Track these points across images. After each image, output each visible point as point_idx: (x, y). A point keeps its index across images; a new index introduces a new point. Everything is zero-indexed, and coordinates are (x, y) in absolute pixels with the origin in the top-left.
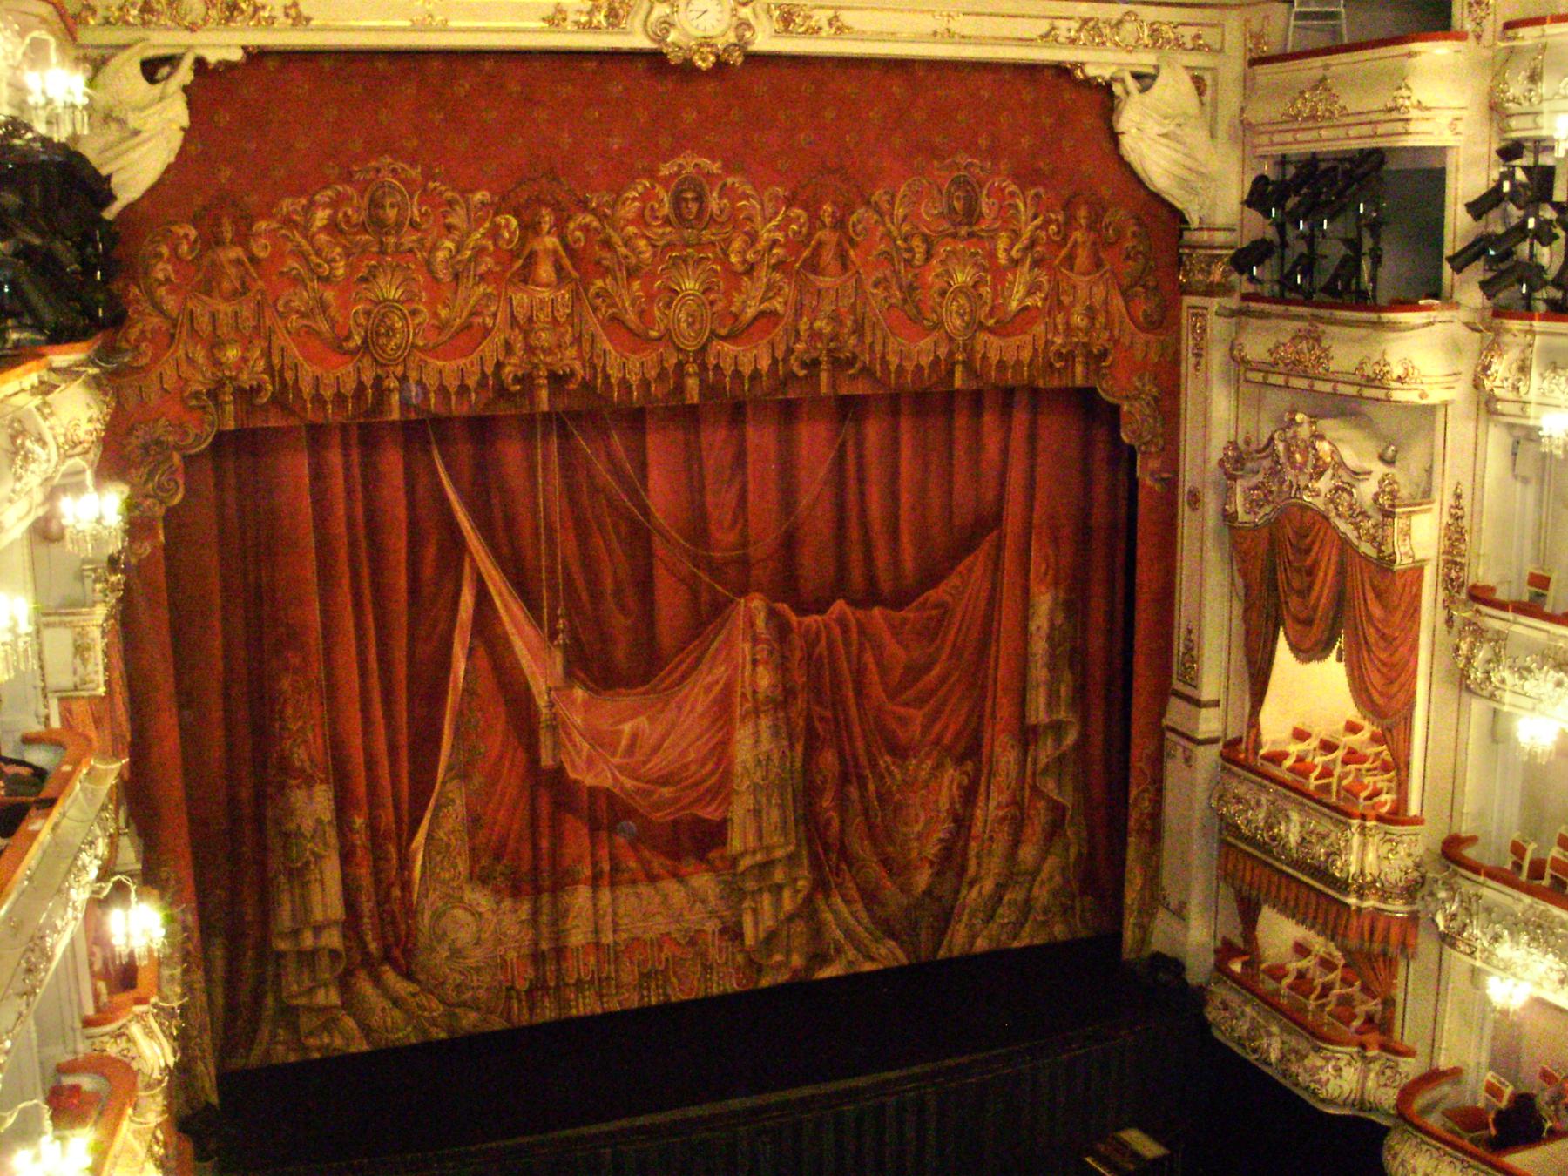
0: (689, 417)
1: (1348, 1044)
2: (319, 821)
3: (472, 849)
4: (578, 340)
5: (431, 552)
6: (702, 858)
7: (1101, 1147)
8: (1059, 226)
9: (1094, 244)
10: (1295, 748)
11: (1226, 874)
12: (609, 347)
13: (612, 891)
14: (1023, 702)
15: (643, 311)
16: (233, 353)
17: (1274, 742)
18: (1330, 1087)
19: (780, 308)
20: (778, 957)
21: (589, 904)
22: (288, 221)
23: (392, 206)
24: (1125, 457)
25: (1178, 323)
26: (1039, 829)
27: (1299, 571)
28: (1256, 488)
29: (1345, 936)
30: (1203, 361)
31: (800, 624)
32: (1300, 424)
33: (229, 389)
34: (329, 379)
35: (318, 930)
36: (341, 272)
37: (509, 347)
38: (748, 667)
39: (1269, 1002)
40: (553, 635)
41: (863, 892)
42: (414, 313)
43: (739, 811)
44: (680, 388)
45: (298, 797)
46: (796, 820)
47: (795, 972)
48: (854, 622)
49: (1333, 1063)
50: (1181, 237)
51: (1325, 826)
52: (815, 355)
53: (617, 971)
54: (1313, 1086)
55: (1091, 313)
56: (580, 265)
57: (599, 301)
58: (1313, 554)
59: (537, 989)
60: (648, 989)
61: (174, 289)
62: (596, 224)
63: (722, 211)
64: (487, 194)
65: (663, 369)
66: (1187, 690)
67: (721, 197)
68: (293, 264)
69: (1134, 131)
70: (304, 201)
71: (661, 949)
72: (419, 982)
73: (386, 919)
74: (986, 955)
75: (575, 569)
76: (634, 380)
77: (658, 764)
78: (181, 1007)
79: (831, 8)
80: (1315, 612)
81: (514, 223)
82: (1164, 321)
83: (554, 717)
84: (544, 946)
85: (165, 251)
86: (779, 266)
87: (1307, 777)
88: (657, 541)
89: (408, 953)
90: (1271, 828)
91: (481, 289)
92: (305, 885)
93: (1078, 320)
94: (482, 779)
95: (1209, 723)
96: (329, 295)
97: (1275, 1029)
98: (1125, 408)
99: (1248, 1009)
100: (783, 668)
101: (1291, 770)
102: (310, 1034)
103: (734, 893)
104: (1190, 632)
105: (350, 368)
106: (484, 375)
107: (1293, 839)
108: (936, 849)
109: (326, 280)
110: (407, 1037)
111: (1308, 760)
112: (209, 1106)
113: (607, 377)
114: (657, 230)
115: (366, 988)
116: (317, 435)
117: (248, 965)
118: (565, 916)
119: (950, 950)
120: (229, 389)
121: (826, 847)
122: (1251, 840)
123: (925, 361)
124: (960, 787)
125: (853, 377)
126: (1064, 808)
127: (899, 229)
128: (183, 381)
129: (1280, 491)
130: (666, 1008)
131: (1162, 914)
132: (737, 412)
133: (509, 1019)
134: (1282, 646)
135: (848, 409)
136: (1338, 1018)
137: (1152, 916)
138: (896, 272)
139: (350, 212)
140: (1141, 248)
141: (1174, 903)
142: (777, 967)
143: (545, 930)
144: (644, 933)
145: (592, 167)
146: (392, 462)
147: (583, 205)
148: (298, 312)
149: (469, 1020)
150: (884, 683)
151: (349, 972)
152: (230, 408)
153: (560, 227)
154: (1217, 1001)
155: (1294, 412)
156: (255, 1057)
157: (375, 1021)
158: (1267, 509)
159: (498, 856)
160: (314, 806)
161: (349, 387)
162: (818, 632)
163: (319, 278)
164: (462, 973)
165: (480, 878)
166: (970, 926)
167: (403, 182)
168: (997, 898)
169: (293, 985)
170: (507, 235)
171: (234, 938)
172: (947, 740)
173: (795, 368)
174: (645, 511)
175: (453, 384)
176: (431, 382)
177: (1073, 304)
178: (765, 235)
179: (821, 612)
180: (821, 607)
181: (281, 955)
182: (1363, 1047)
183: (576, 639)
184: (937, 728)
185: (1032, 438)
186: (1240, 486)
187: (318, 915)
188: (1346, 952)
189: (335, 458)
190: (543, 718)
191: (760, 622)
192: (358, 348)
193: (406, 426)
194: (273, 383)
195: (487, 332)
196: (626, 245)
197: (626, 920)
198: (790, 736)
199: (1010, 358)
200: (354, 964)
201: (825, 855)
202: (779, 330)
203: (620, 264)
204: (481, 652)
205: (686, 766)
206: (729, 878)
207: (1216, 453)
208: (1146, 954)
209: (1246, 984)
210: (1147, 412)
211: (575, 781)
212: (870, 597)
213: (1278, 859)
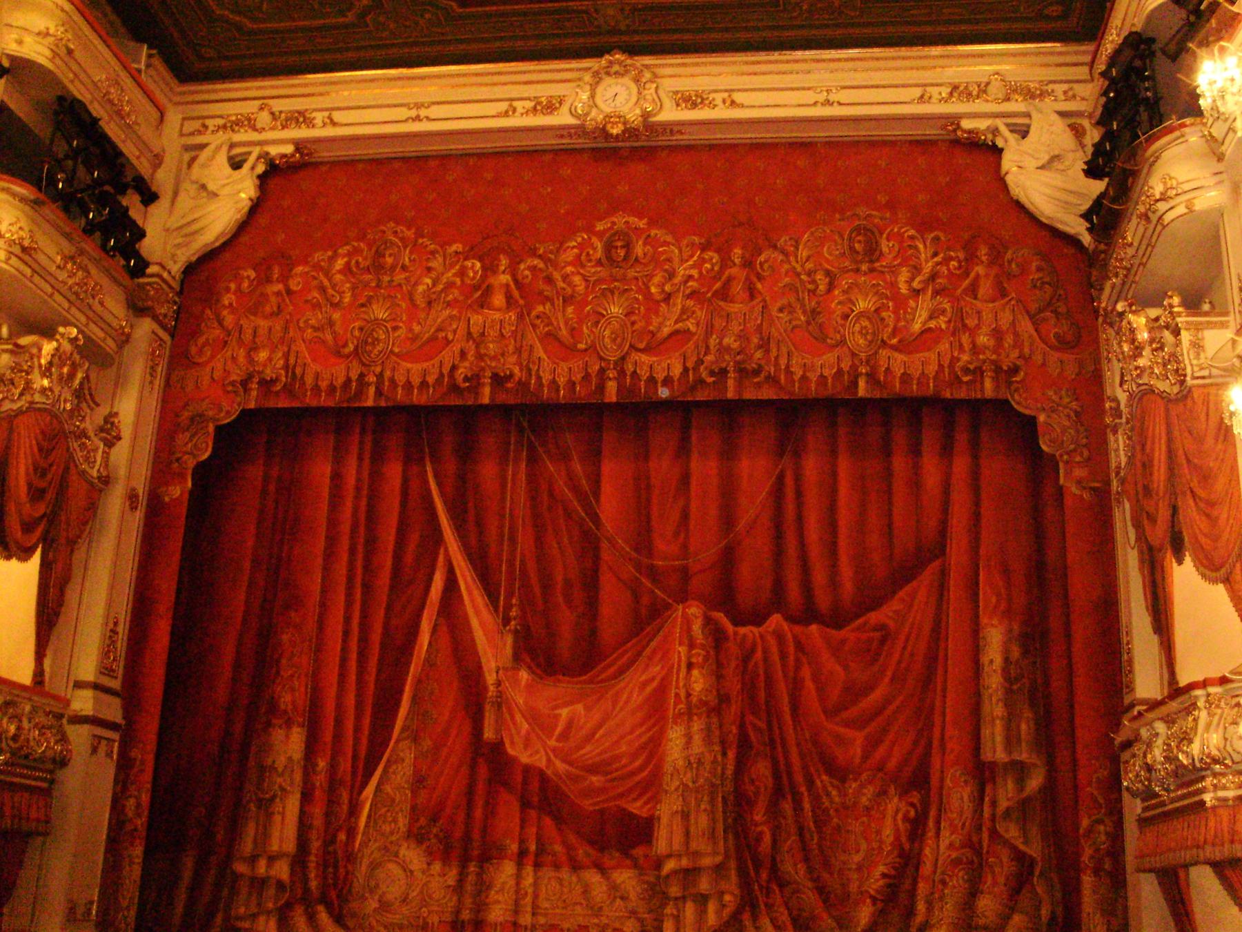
2: (290, 759)
3: (413, 808)
4: (518, 351)
5: (414, 538)
6: (626, 853)
8: (960, 262)
12: (544, 356)
13: (535, 872)
14: (977, 737)
15: (573, 329)
16: (263, 355)
19: (693, 328)
21: (512, 882)
22: (317, 267)
23: (390, 255)
26: (1002, 880)
31: (736, 634)
33: (256, 380)
34: (327, 376)
35: (272, 859)
36: (347, 300)
37: (463, 354)
40: (506, 621)
42: (395, 329)
43: (667, 809)
44: (601, 388)
45: (278, 735)
48: (789, 635)
52: (724, 365)
55: (998, 334)
56: (524, 296)
62: (542, 265)
67: (645, 244)
69: (1015, 169)
70: (330, 253)
73: (328, 860)
75: (531, 566)
76: (562, 381)
77: (590, 752)
79: (726, 91)
81: (478, 265)
84: (466, 915)
85: (233, 286)
86: (693, 295)
88: (605, 544)
89: (344, 897)
92: (270, 815)
94: (429, 743)
96: (336, 316)
98: (1042, 418)
100: (718, 675)
105: (343, 366)
106: (441, 375)
109: (335, 306)
113: (539, 378)
114: (591, 269)
118: (489, 887)
120: (256, 380)
121: (758, 865)
124: (906, 818)
126: (1032, 861)
127: (802, 266)
140: (1047, 280)
143: (468, 902)
145: (542, 226)
147: (534, 253)
148: (313, 327)
150: (823, 699)
151: (288, 906)
152: (254, 393)
159: (434, 819)
160: (289, 745)
162: (754, 646)
163: (332, 304)
165: (416, 836)
172: (892, 764)
173: (704, 375)
174: (596, 520)
176: (401, 379)
177: (978, 327)
178: (681, 272)
180: (758, 619)
181: (237, 877)
183: (527, 628)
184: (881, 750)
185: (975, 475)
187: (275, 847)
191: (697, 628)
194: (287, 377)
195: (448, 342)
196: (564, 281)
198: (724, 744)
202: (691, 344)
205: (618, 758)
206: (652, 879)
210: (1067, 423)
212: (808, 614)
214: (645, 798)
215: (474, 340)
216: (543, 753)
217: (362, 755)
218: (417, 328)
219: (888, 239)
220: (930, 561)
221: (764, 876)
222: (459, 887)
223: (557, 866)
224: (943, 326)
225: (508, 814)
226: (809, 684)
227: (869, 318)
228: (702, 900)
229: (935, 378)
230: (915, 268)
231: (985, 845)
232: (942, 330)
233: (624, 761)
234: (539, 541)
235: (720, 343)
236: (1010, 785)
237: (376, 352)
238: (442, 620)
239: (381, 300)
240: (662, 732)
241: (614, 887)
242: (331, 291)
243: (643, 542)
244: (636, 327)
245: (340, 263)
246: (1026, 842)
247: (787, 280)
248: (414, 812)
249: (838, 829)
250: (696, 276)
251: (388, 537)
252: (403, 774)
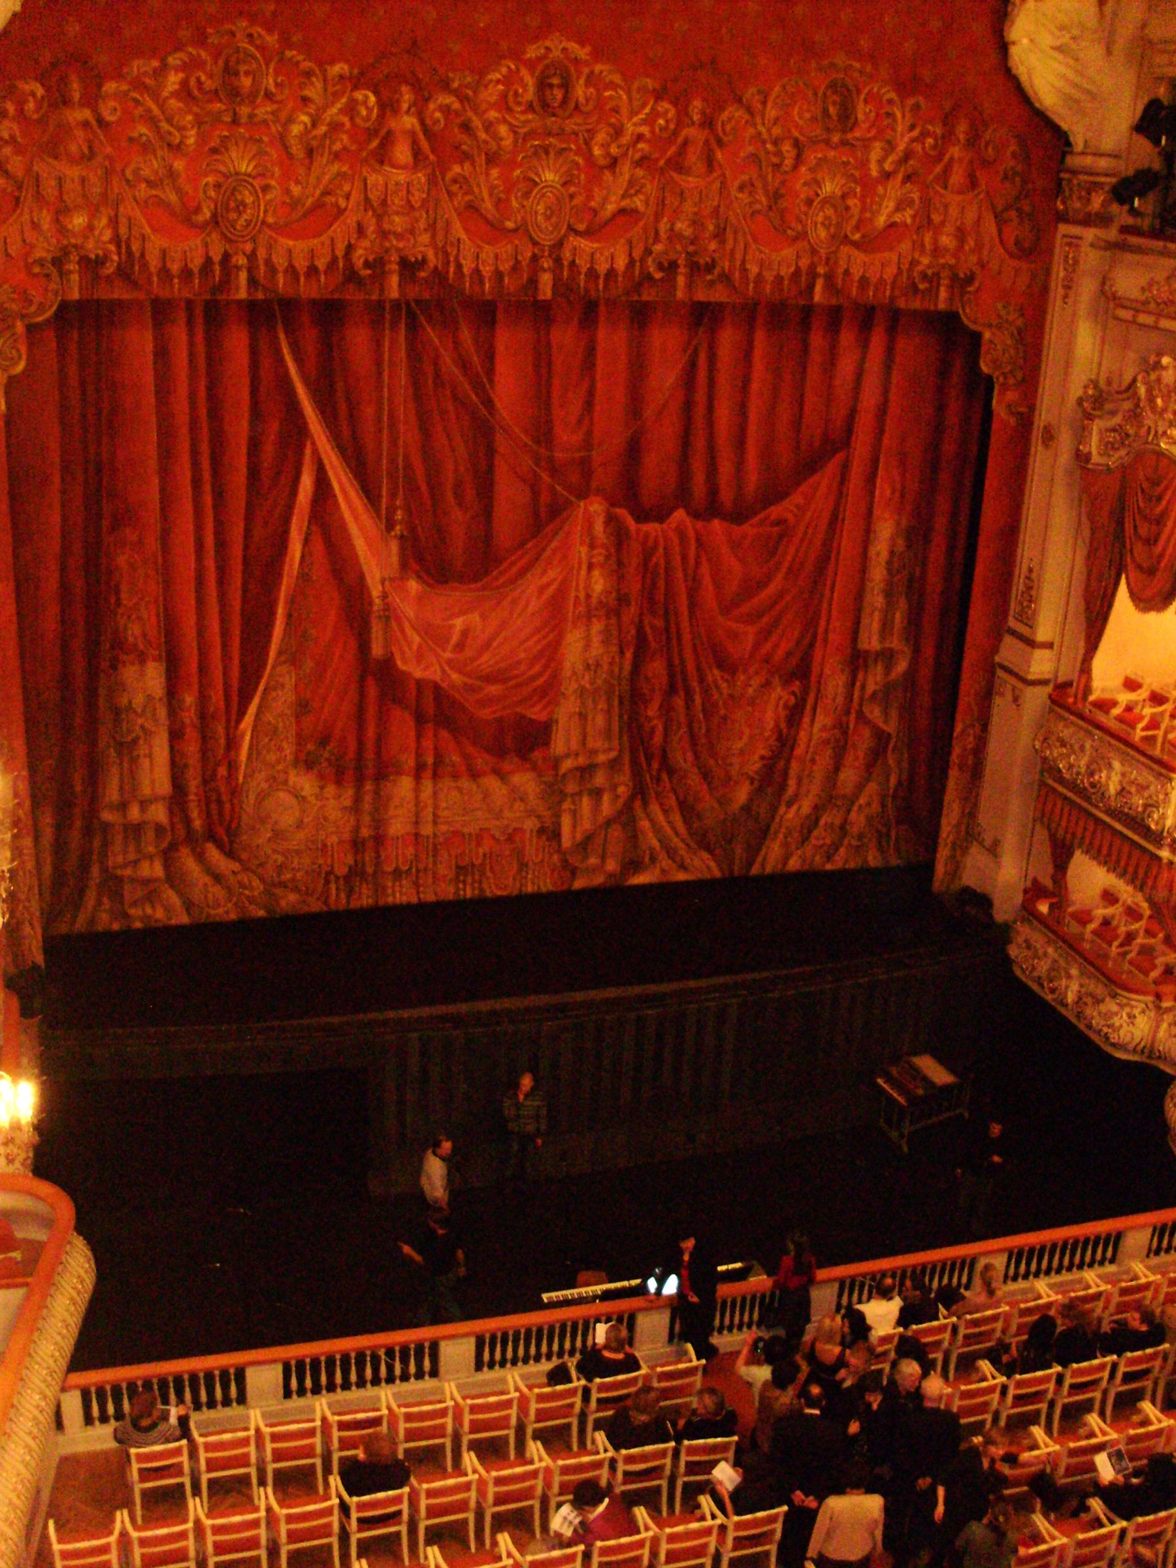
0: (541, 314)
1: (1144, 993)
3: (299, 735)
4: (432, 227)
7: (894, 1071)
9: (971, 162)
10: (1124, 698)
11: (1043, 816)
12: (463, 236)
16: (79, 221)
17: (1103, 690)
18: (1122, 1033)
20: (593, 861)
22: (138, 84)
23: (247, 73)
24: (980, 389)
25: (1050, 252)
26: (861, 754)
27: (1146, 519)
28: (1114, 430)
29: (1154, 887)
30: (1071, 293)
31: (638, 531)
32: (1165, 368)
33: (74, 257)
35: (144, 804)
37: (361, 230)
38: (584, 572)
39: (1072, 946)
40: (390, 526)
41: (682, 804)
42: (266, 189)
43: (565, 712)
44: (533, 282)
45: (129, 673)
46: (621, 728)
47: (611, 875)
49: (1127, 1009)
50: (1062, 161)
51: (1145, 777)
53: (435, 863)
54: (1105, 1030)
55: (961, 234)
56: (438, 150)
57: (455, 188)
58: (1164, 503)
59: (355, 873)
60: (464, 882)
61: (19, 150)
62: (457, 106)
63: (587, 100)
64: (346, 67)
65: (518, 262)
66: (1021, 628)
69: (1025, 41)
70: (155, 63)
71: (478, 844)
72: (239, 860)
73: (210, 799)
74: (798, 875)
76: (487, 270)
77: (487, 661)
78: (10, 871)
80: (1159, 563)
82: (1035, 251)
83: (387, 607)
84: (365, 832)
85: (11, 108)
87: (1134, 728)
89: (232, 832)
90: (1092, 774)
91: (335, 168)
92: (134, 761)
93: (946, 240)
95: (1041, 664)
96: (179, 165)
97: (1074, 972)
98: (987, 335)
99: (1050, 950)
100: (618, 573)
101: (1119, 719)
102: (134, 904)
103: (554, 793)
104: (1031, 570)
105: (198, 242)
106: (334, 259)
107: (1113, 789)
108: (758, 765)
109: (176, 149)
110: (227, 912)
111: (1137, 710)
112: (35, 967)
113: (459, 266)
115: (190, 864)
116: (161, 310)
117: (75, 838)
119: (763, 866)
120: (74, 257)
121: (649, 757)
122: (1072, 786)
123: (786, 271)
124: (786, 706)
125: (711, 283)
127: (769, 130)
128: (28, 247)
129: (1136, 434)
130: (481, 903)
131: (974, 849)
132: (589, 312)
133: (326, 903)
134: (1123, 592)
135: (703, 316)
136: (1138, 967)
137: (965, 851)
138: (763, 177)
139: (203, 78)
141: (987, 843)
142: (594, 870)
143: (366, 819)
144: (466, 829)
146: (237, 341)
147: (446, 86)
148: (147, 181)
149: (289, 901)
151: (173, 847)
152: (75, 278)
154: (1020, 940)
155: (1160, 354)
156: (81, 924)
157: (196, 895)
158: (1123, 452)
160: (145, 682)
161: (196, 263)
164: (283, 854)
165: (308, 764)
166: (786, 845)
167: (257, 48)
168: (812, 822)
169: (118, 856)
170: (364, 112)
171: (64, 808)
174: (489, 403)
175: (301, 264)
176: (280, 261)
177: (943, 223)
178: (630, 128)
179: (661, 519)
181: (106, 827)
182: (1159, 997)
183: (412, 529)
184: (768, 646)
186: (1096, 427)
188: (1153, 904)
189: (179, 335)
190: (375, 608)
191: (599, 527)
192: (207, 223)
193: (251, 306)
194: (119, 254)
195: (341, 212)
197: (446, 813)
199: (873, 276)
200: (178, 839)
201: (645, 762)
203: (479, 147)
204: (318, 546)
207: (1076, 392)
208: (956, 886)
209: (1052, 927)
210: (1009, 342)
211: (403, 672)
212: (711, 509)
213: (1097, 807)
214: (544, 701)
215: (374, 211)
216: (437, 667)
217: (235, 684)
218: (296, 190)
219: (866, 102)
220: (834, 453)
221: (655, 765)
222: (356, 808)
223: (456, 776)
224: (909, 221)
225: (402, 726)
226: (707, 581)
227: (834, 206)
228: (597, 793)
229: (894, 283)
230: (889, 142)
231: (851, 726)
232: (906, 225)
233: (523, 667)
234: (426, 433)
235: (672, 230)
236: (879, 669)
237: (242, 222)
238: (314, 528)
239: (241, 145)
240: (561, 636)
241: (513, 790)
242: (165, 126)
243: (543, 432)
244: (575, 202)
245: (173, 80)
246: (886, 722)
247: (751, 149)
248: (300, 740)
249: (724, 718)
250: (648, 135)
251: (239, 428)
252: (284, 699)
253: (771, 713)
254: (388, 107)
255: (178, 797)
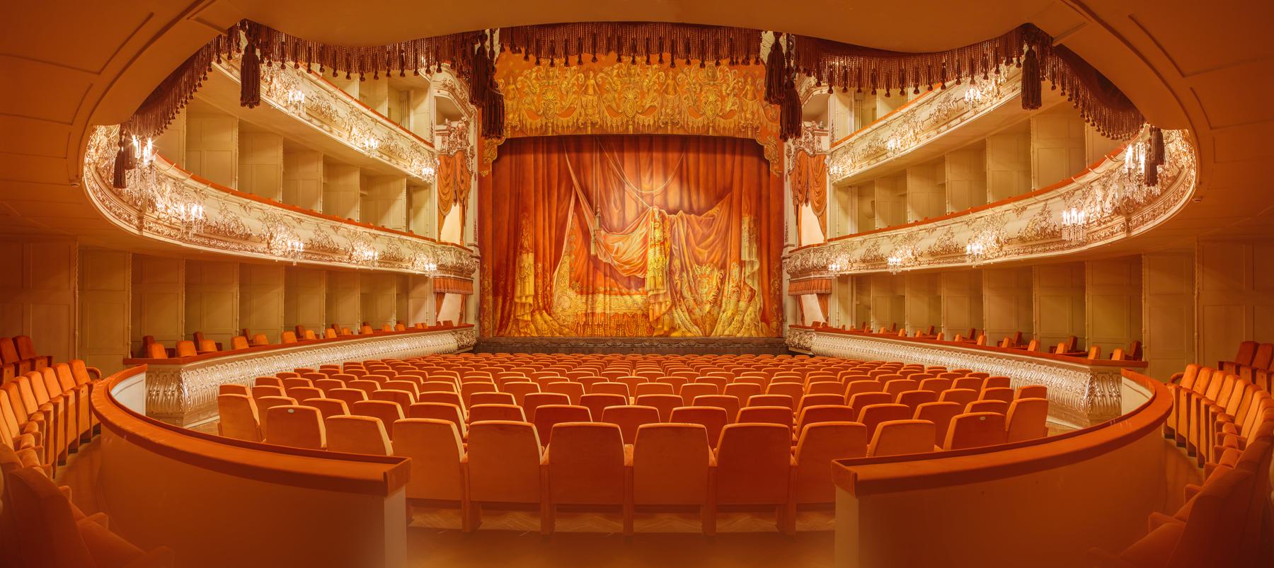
43: (649, 275)
45: (525, 256)
55: (753, 113)
56: (600, 89)
59: (586, 324)
68: (526, 89)
77: (625, 258)
93: (749, 116)
115: (538, 317)
147: (601, 71)
153: (595, 77)
160: (528, 259)
253: (715, 281)
254: (587, 77)
255: (536, 296)
